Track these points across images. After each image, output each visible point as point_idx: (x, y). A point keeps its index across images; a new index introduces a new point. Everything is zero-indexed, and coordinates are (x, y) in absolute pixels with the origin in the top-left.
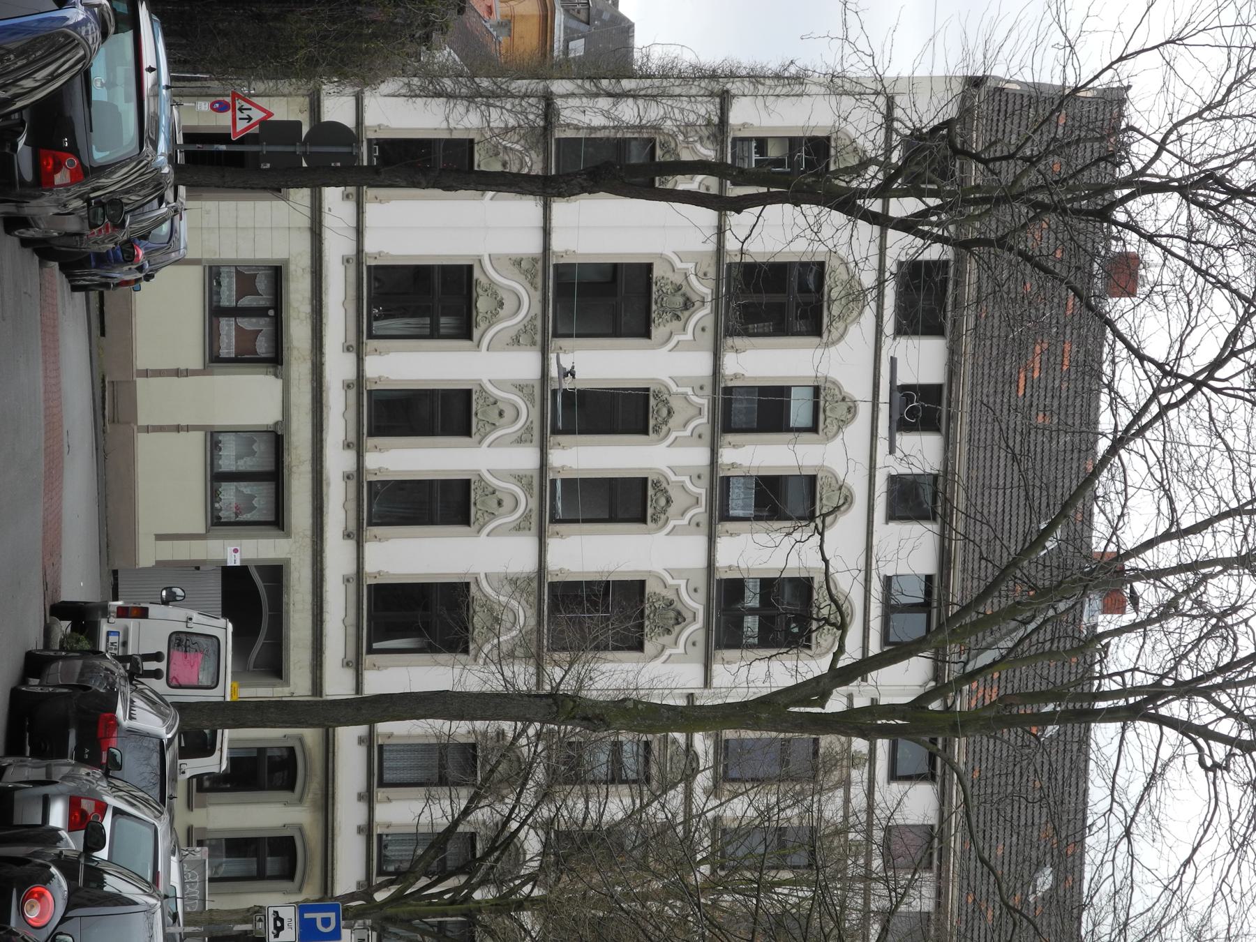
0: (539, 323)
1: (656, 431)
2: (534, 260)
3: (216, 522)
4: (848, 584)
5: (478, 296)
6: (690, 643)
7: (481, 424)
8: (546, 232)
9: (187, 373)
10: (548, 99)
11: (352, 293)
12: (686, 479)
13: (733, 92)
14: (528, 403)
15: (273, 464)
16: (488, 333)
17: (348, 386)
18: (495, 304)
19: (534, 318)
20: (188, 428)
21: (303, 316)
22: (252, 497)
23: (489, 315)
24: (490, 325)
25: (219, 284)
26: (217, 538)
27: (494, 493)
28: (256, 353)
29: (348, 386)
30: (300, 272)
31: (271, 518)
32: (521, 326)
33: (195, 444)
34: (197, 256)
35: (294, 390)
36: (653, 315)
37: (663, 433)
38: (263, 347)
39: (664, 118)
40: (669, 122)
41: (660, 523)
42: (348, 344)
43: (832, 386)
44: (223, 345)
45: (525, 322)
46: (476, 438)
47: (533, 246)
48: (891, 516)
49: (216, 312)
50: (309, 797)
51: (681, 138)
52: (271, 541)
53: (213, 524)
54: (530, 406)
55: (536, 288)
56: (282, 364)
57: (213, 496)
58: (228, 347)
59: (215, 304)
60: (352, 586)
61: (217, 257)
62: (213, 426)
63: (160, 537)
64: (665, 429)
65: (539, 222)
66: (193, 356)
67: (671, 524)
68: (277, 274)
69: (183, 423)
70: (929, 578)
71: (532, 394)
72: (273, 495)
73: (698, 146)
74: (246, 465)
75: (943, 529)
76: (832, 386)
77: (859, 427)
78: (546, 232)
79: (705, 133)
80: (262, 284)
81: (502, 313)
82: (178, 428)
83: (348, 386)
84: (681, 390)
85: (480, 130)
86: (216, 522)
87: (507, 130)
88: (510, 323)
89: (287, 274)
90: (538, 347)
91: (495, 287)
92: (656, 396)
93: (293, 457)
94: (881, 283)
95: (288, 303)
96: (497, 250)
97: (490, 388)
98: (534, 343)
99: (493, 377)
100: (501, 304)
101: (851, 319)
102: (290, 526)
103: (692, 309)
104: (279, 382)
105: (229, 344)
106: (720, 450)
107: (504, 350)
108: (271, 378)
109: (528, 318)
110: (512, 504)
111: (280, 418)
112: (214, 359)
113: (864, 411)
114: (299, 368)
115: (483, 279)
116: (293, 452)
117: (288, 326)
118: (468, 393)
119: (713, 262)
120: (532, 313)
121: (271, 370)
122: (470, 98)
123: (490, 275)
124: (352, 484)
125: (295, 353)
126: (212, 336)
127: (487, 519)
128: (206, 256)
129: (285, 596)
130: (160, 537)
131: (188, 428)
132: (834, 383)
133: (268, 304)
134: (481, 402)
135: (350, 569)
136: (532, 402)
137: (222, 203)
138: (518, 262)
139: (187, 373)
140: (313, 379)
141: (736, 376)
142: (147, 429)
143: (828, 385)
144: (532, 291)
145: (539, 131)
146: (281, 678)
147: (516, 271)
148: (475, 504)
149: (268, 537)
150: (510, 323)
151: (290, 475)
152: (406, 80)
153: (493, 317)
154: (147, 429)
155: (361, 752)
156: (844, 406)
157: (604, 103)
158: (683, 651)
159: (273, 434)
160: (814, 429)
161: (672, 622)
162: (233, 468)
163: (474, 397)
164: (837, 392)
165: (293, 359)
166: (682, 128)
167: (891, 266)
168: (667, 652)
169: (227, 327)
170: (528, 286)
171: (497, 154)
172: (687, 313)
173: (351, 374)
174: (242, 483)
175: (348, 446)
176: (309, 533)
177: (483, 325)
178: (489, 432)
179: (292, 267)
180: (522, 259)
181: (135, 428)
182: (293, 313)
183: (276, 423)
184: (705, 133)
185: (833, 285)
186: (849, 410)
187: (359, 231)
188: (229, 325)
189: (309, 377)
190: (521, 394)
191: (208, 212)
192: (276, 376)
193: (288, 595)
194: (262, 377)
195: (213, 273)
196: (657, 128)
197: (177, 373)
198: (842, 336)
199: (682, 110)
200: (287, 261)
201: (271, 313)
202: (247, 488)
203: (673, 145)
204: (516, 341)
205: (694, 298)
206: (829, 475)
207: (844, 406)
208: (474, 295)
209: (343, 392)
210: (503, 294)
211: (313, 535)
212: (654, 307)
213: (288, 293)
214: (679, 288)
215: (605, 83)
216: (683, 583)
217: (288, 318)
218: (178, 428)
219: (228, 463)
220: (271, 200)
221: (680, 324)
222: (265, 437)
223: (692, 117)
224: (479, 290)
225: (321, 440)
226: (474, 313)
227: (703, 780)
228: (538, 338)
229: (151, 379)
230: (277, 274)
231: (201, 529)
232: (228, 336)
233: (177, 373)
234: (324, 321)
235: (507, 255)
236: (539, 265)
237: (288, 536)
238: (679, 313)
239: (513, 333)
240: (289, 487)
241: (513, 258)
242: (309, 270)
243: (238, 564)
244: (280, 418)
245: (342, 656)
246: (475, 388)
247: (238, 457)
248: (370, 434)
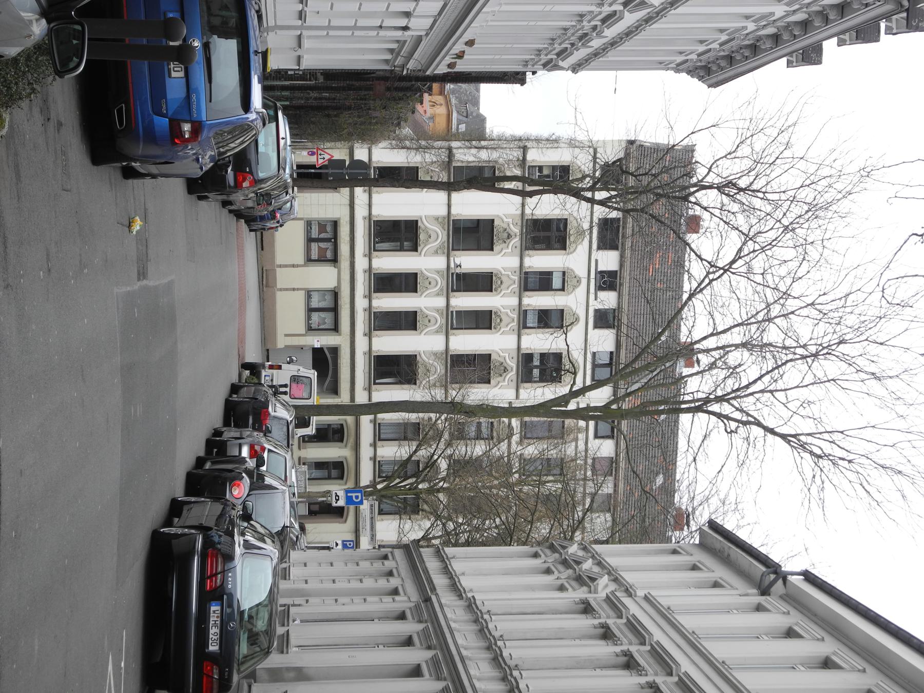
4: (577, 356)
10: (450, 149)
12: (509, 311)
13: (529, 146)
32: (438, 246)
39: (499, 158)
40: (501, 159)
41: (498, 329)
46: (419, 293)
47: (443, 212)
48: (596, 326)
50: (349, 445)
51: (506, 166)
55: (445, 230)
64: (499, 289)
67: (502, 330)
70: (611, 353)
71: (442, 313)
73: (514, 169)
75: (617, 332)
84: (506, 273)
85: (421, 163)
87: (432, 163)
88: (434, 245)
92: (495, 313)
94: (591, 227)
98: (444, 253)
100: (430, 237)
110: (435, 283)
115: (422, 226)
122: (417, 149)
123: (425, 224)
129: (339, 360)
133: (331, 237)
138: (437, 219)
144: (443, 231)
145: (446, 163)
152: (390, 142)
155: (371, 464)
156: (576, 280)
157: (474, 151)
167: (596, 220)
168: (504, 251)
170: (441, 229)
171: (428, 173)
177: (422, 246)
184: (517, 164)
196: (496, 162)
198: (575, 250)
199: (507, 154)
201: (333, 240)
203: (503, 169)
205: (512, 234)
207: (576, 280)
212: (495, 238)
214: (505, 230)
215: (474, 142)
216: (507, 355)
223: (511, 157)
227: (516, 438)
228: (446, 251)
243: (319, 347)
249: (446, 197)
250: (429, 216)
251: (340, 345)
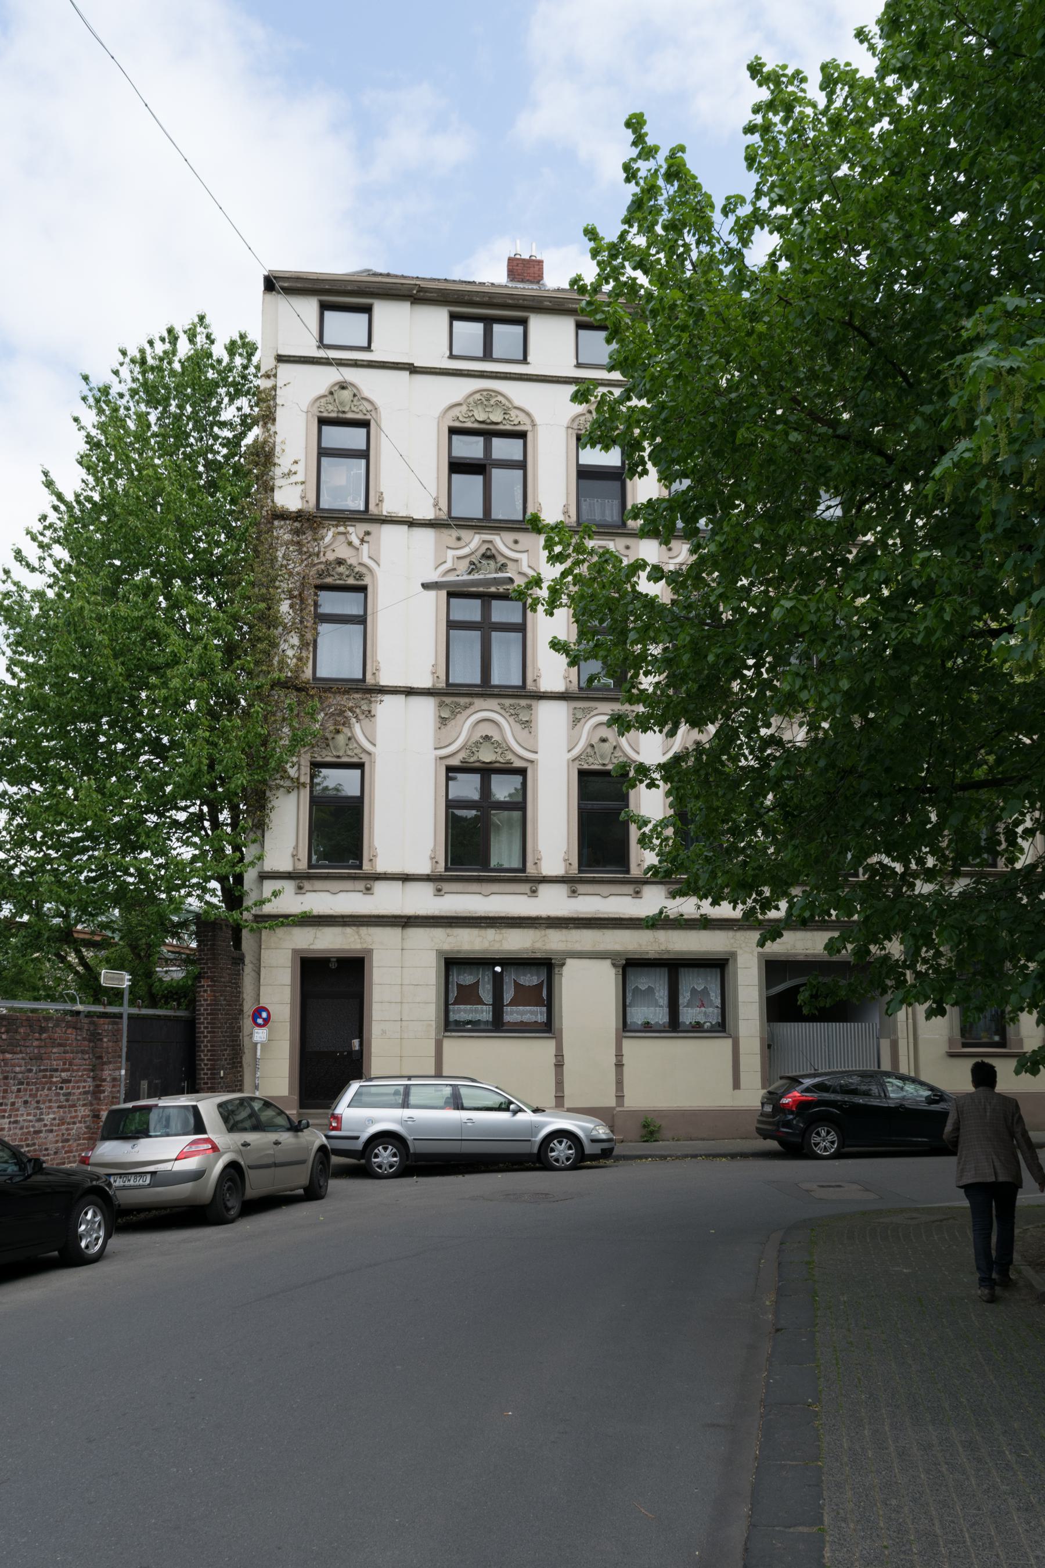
0: (507, 702)
1: (360, 576)
2: (441, 705)
3: (723, 1027)
5: (479, 761)
6: (462, 543)
7: (349, 753)
8: (410, 692)
9: (559, 1056)
11: (474, 887)
14: (592, 714)
15: (714, 970)
16: (518, 750)
17: (574, 893)
18: (487, 744)
19: (503, 707)
20: (619, 1055)
21: (498, 937)
22: (694, 991)
23: (499, 750)
24: (510, 749)
25: (469, 1022)
26: (737, 1026)
27: (592, 746)
28: (541, 985)
29: (574, 892)
30: (451, 939)
31: (718, 970)
32: (511, 720)
33: (635, 1049)
34: (432, 1044)
35: (577, 947)
36: (501, 590)
37: (363, 570)
38: (530, 979)
42: (528, 891)
43: (576, 423)
44: (533, 1019)
45: (507, 715)
46: (365, 758)
49: (498, 1026)
52: (740, 972)
53: (724, 1031)
54: (595, 712)
55: (470, 704)
56: (551, 959)
57: (697, 1029)
58: (535, 1014)
59: (490, 1027)
60: (446, 887)
61: (433, 1023)
62: (617, 1030)
63: (736, 1085)
65: (401, 699)
66: (543, 1049)
67: (366, 560)
68: (452, 964)
69: (613, 1060)
70: (580, 326)
71: (583, 709)
72: (691, 969)
74: (662, 995)
76: (576, 423)
77: (515, 392)
78: (410, 692)
79: (309, 535)
80: (467, 979)
81: (497, 737)
82: (619, 1066)
83: (574, 893)
86: (723, 1027)
88: (509, 731)
89: (452, 952)
90: (534, 703)
91: (469, 743)
93: (650, 948)
95: (484, 951)
96: (430, 742)
97: (576, 752)
98: (529, 707)
99: (565, 749)
100: (487, 738)
101: (507, 403)
102: (726, 952)
103: (494, 551)
104: (570, 962)
105: (532, 1013)
106: (385, 513)
107: (536, 737)
108: (566, 970)
109: (502, 712)
111: (608, 962)
112: (548, 1028)
113: (350, 375)
114: (554, 941)
116: (644, 948)
117: (509, 952)
118: (582, 774)
119: (446, 532)
120: (498, 708)
121: (556, 970)
124: (581, 888)
125: (539, 945)
126: (524, 1029)
127: (620, 754)
128: (433, 1034)
130: (736, 1085)
131: (619, 1055)
132: (573, 420)
134: (591, 760)
135: (428, 888)
136: (590, 710)
137: (374, 1018)
138: (443, 721)
139: (559, 1056)
140: (566, 928)
141: (566, 513)
142: (620, 1098)
143: (575, 426)
146: (727, 960)
147: (453, 722)
148: (604, 765)
149: (736, 974)
150: (509, 731)
151: (668, 952)
153: (501, 746)
154: (620, 1098)
158: (526, 554)
159: (629, 970)
160: (522, 435)
161: (492, 562)
162: (666, 1010)
163: (586, 767)
164: (582, 418)
165: (544, 948)
166: (304, 557)
169: (513, 1014)
170: (469, 711)
172: (500, 559)
173: (562, 890)
174: (681, 1001)
175: (368, 890)
176: (731, 934)
177: (510, 756)
178: (623, 752)
179: (446, 947)
180: (440, 717)
181: (618, 1109)
182: (496, 947)
183: (614, 965)
185: (473, 419)
186: (343, 388)
187: (406, 878)
188: (512, 1013)
189: (564, 932)
190: (583, 721)
191: (384, 1032)
192: (563, 964)
193: (796, 955)
194: (564, 980)
195: (450, 1026)
197: (559, 1066)
198: (528, 414)
200: (439, 952)
202: (684, 998)
203: (322, 566)
204: (527, 724)
205: (483, 550)
206: (317, 404)
208: (477, 764)
209: (580, 897)
210: (477, 736)
211: (732, 929)
213: (473, 952)
216: (451, 553)
217: (502, 952)
218: (619, 1066)
219: (659, 1015)
220: (736, 969)
221: (510, 564)
222: (631, 977)
224: (472, 760)
225: (631, 919)
226: (497, 765)
228: (523, 702)
229: (566, 1093)
230: (452, 964)
231: (726, 1045)
232: (522, 1013)
233: (559, 1066)
234: (503, 915)
235: (436, 731)
236: (448, 700)
237: (733, 955)
238: (499, 565)
239: (518, 727)
240: (681, 952)
241: (439, 725)
242: (449, 931)
244: (608, 962)
245: (629, 898)
246: (576, 766)
247: (657, 1005)
248: (628, 872)
249: (388, 699)
250: (437, 739)
251: (295, 951)
